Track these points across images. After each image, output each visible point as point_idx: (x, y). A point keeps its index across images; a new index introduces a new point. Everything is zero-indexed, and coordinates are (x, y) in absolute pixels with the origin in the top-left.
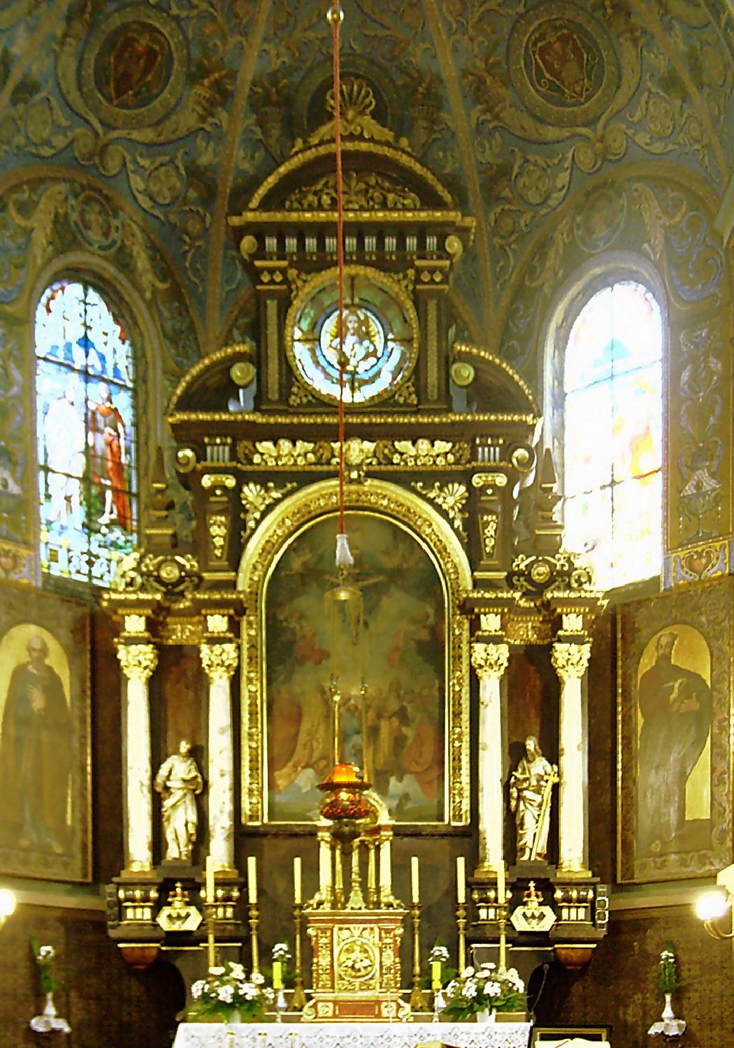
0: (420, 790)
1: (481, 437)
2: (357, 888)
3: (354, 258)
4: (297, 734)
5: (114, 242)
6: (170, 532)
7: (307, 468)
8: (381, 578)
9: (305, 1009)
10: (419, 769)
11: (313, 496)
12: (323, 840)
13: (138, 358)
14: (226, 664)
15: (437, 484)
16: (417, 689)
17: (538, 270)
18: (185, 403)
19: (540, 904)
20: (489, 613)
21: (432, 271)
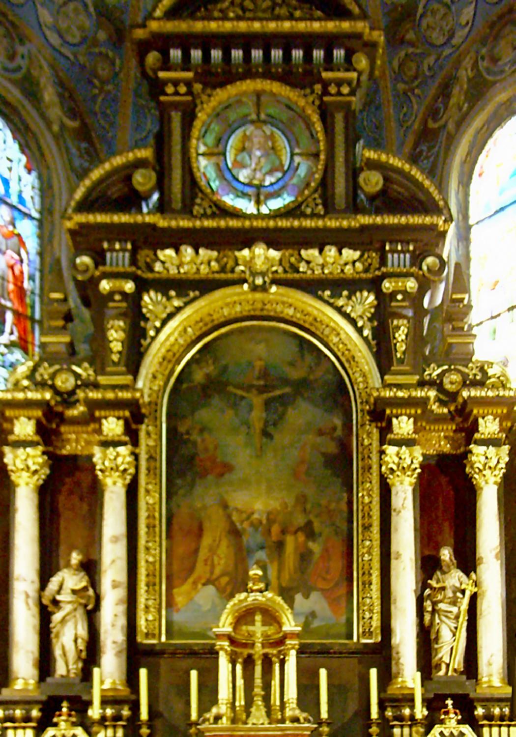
1: (391, 242)
2: (260, 703)
3: (260, 70)
4: (196, 551)
5: (19, 68)
6: (67, 339)
7: (211, 276)
8: (287, 390)
11: (216, 304)
12: (222, 649)
13: (46, 190)
14: (122, 468)
15: (345, 293)
16: (324, 502)
17: (442, 110)
18: (85, 206)
19: (459, 722)
20: (401, 415)
21: (339, 83)
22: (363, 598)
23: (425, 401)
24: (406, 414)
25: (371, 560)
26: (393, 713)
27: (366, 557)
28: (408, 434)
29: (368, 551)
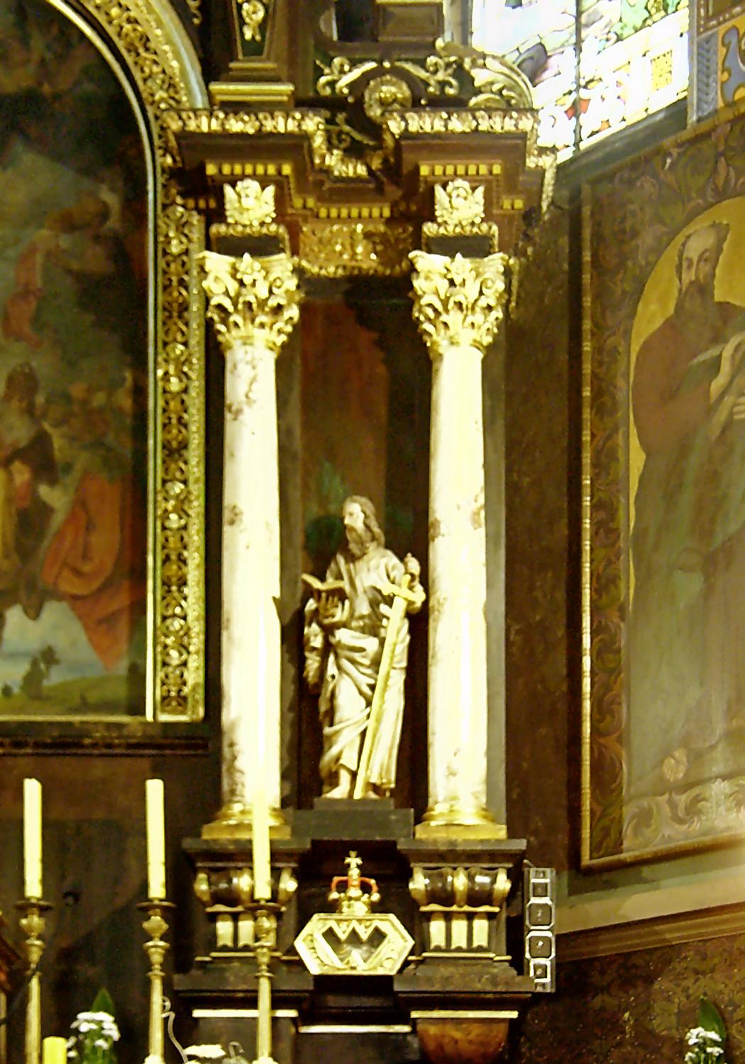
0: (82, 637)
10: (78, 588)
16: (77, 390)
19: (375, 908)
20: (243, 177)
23: (296, 146)
24: (254, 176)
25: (185, 528)
26: (210, 884)
28: (262, 224)
29: (174, 506)
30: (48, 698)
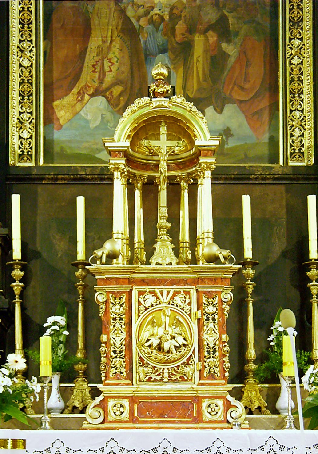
2: (165, 237)
9: (89, 410)
22: (291, 111)
27: (296, 61)
30: (228, 154)
